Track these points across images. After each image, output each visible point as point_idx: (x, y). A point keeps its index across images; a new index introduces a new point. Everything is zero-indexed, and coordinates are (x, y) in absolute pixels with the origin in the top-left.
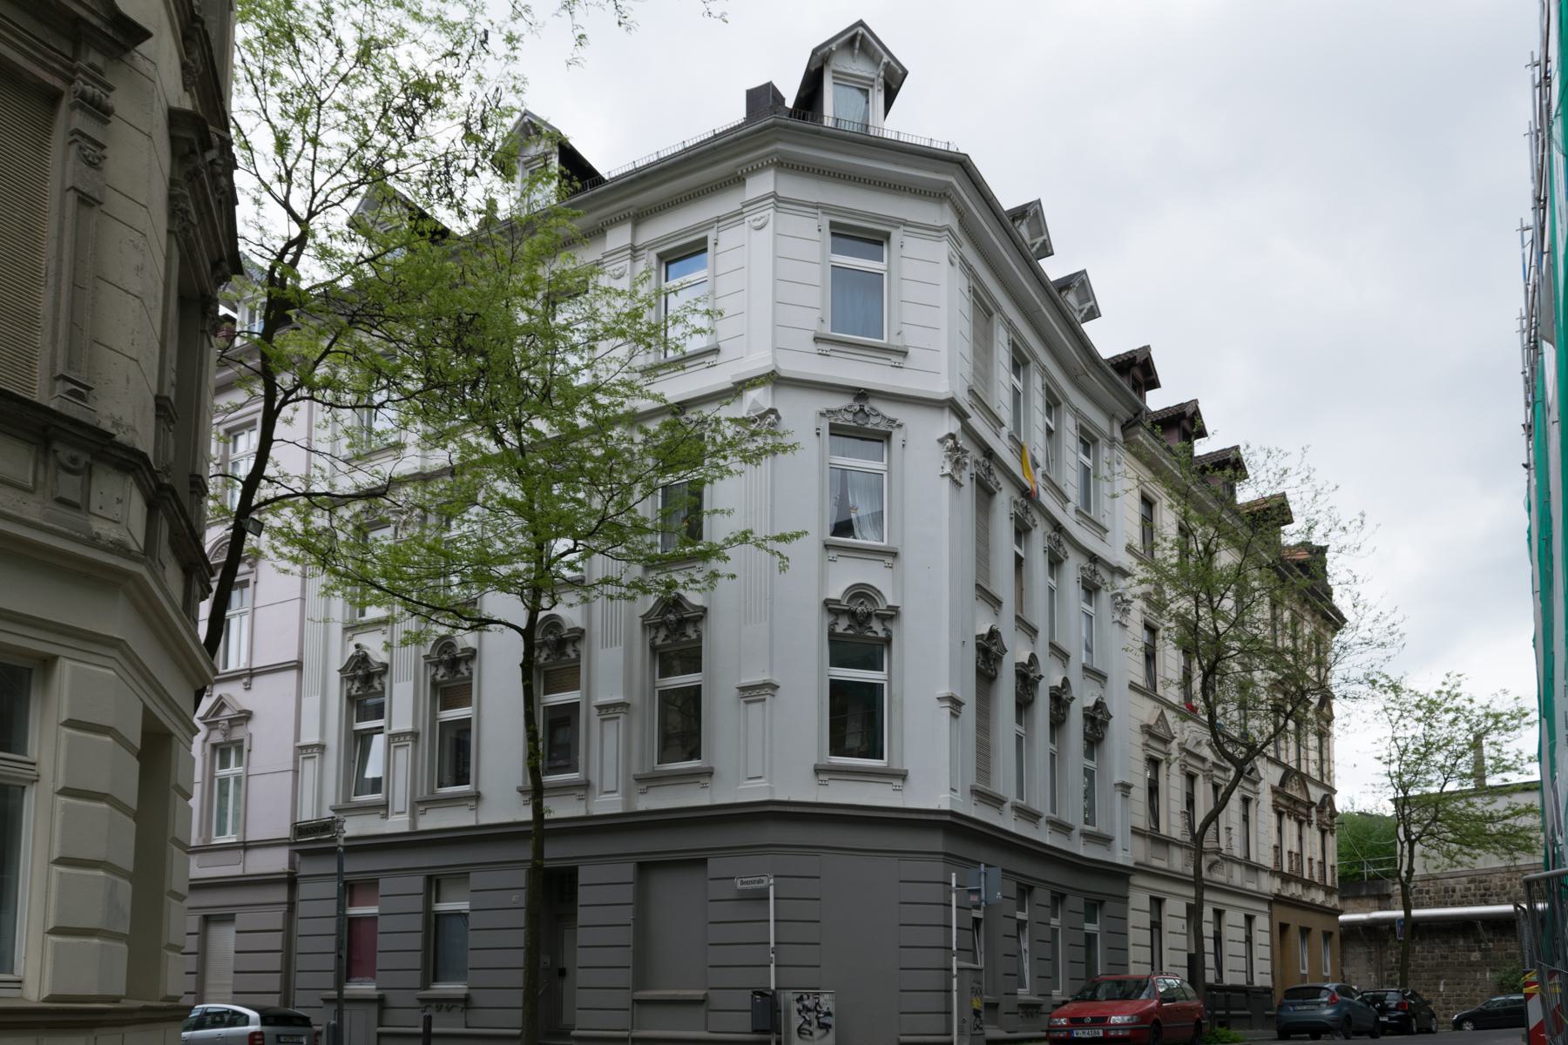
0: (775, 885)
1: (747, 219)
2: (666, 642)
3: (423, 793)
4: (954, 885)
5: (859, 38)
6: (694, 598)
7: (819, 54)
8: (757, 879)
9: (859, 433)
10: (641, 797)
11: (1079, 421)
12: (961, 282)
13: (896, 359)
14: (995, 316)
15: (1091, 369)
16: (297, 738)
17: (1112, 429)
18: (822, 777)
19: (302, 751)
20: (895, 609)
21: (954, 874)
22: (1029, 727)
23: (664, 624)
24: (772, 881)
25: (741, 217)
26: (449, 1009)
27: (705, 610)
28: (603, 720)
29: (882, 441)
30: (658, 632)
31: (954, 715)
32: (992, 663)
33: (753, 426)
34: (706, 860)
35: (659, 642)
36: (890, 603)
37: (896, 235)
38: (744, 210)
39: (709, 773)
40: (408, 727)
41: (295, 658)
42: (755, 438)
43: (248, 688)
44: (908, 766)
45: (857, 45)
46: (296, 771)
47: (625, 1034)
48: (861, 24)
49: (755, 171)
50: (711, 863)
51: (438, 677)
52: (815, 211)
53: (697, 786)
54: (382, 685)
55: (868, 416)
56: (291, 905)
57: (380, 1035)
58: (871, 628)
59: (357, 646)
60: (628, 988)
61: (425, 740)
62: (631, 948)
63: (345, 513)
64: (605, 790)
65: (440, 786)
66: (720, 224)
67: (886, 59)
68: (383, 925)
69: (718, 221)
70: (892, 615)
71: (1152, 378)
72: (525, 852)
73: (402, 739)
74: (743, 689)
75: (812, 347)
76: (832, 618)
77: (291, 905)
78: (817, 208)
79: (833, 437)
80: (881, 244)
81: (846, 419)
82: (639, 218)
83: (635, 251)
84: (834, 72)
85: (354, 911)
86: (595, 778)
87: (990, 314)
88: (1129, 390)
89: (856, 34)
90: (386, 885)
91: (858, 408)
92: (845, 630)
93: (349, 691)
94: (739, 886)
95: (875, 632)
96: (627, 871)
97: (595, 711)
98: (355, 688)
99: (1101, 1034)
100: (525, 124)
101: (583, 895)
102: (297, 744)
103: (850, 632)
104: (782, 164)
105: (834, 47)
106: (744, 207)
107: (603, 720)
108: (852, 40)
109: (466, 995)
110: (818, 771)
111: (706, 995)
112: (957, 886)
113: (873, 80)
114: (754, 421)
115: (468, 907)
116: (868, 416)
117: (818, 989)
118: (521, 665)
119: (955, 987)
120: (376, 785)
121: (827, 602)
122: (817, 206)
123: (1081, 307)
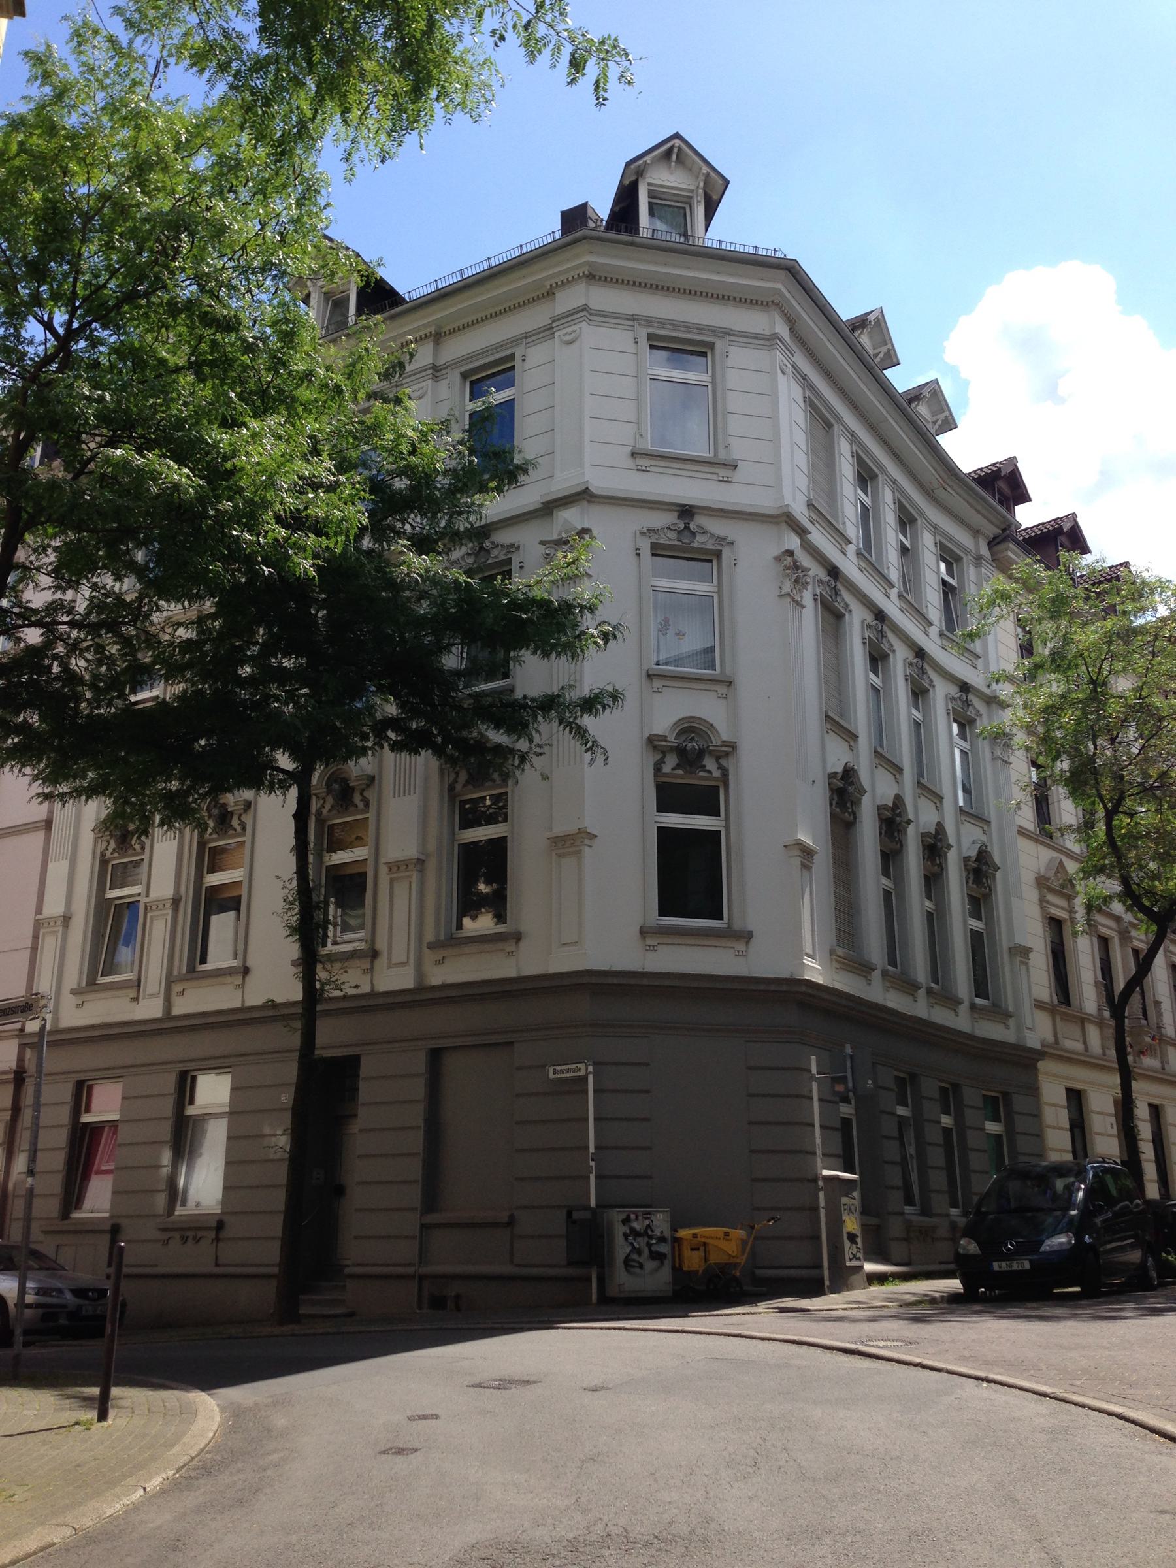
0: (595, 1074)
1: (556, 334)
5: (675, 150)
11: (938, 538)
12: (797, 392)
13: (724, 473)
18: (650, 941)
24: (591, 1069)
31: (806, 867)
37: (719, 344)
38: (554, 325)
45: (674, 157)
46: (34, 949)
48: (677, 136)
52: (631, 323)
64: (394, 961)
69: (526, 338)
75: (630, 463)
78: (633, 320)
80: (704, 355)
84: (649, 184)
86: (381, 944)
87: (829, 426)
89: (673, 147)
91: (682, 526)
94: (551, 1076)
95: (710, 772)
98: (328, 807)
103: (680, 772)
104: (594, 277)
118: (293, 816)
122: (633, 318)
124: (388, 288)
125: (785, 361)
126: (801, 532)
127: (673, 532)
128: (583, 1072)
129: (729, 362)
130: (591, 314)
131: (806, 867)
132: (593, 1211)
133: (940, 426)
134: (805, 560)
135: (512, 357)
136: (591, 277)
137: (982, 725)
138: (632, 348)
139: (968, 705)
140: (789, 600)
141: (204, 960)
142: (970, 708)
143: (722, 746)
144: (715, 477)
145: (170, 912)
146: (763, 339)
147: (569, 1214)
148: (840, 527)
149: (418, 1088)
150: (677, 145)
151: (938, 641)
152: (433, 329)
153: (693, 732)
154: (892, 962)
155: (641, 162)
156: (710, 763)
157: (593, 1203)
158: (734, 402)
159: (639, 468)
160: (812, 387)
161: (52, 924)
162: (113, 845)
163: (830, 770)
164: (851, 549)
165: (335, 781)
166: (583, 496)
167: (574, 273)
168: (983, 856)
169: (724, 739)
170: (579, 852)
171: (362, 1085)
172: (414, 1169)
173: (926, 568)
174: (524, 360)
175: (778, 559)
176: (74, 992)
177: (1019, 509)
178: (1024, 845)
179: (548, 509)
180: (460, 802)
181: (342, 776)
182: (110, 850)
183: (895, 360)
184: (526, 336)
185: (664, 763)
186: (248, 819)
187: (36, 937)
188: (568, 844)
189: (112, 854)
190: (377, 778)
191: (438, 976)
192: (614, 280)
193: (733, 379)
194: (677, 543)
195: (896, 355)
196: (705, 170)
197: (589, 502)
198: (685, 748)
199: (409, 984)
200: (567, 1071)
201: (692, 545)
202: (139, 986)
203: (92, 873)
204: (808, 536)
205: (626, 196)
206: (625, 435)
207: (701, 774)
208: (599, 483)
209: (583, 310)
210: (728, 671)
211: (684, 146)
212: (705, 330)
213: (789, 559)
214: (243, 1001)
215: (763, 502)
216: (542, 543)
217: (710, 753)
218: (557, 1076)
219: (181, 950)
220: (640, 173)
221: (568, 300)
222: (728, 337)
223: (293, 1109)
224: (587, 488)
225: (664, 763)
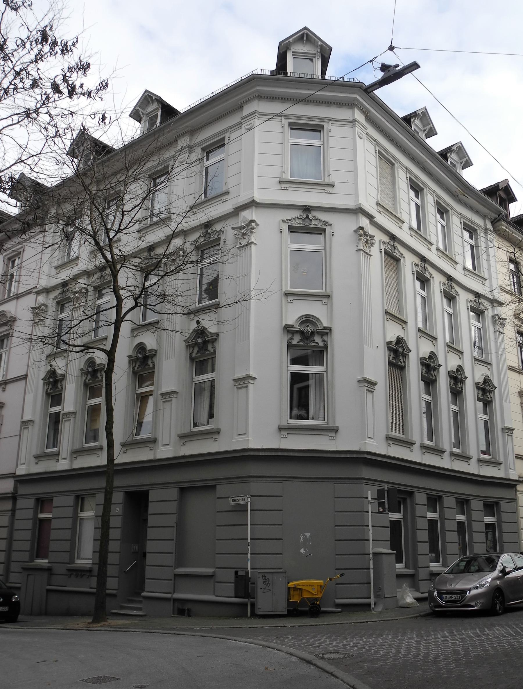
1: (243, 126)
3: (77, 447)
4: (370, 499)
5: (305, 35)
6: (212, 329)
8: (241, 498)
9: (307, 230)
10: (183, 447)
11: (462, 220)
12: (371, 147)
13: (327, 189)
14: (396, 165)
15: (465, 191)
16: (22, 418)
17: (485, 223)
18: (283, 433)
19: (25, 424)
20: (330, 329)
22: (435, 397)
23: (196, 344)
24: (249, 499)
25: (240, 125)
26: (82, 576)
27: (217, 335)
29: (321, 234)
30: (193, 350)
32: (401, 358)
33: (243, 231)
34: (215, 485)
35: (194, 355)
36: (325, 324)
37: (326, 125)
38: (242, 121)
39: (218, 432)
41: (25, 373)
42: (244, 237)
43: (4, 390)
44: (338, 423)
45: (305, 38)
47: (169, 596)
48: (306, 28)
49: (248, 101)
50: (55, 499)
52: (280, 118)
53: (212, 440)
55: (311, 220)
56: (13, 511)
57: (48, 591)
58: (314, 340)
60: (172, 566)
61: (79, 416)
62: (175, 541)
63: (52, 295)
64: (163, 444)
66: (231, 130)
67: (320, 43)
68: (54, 524)
69: (230, 129)
70: (327, 331)
71: (511, 196)
74: (236, 380)
75: (278, 186)
76: (290, 336)
77: (13, 511)
79: (291, 233)
80: (319, 131)
81: (299, 223)
82: (193, 132)
83: (191, 149)
84: (293, 52)
87: (393, 164)
88: (498, 206)
89: (304, 33)
90: (57, 501)
91: (305, 217)
93: (47, 391)
94: (232, 503)
95: (317, 343)
96: (173, 493)
97: (160, 396)
100: (146, 96)
101: (152, 508)
102: (22, 420)
103: (302, 343)
104: (261, 97)
105: (291, 40)
106: (242, 120)
108: (302, 36)
109: (90, 568)
111: (214, 572)
112: (371, 498)
113: (315, 54)
114: (244, 228)
115: (93, 514)
116: (311, 220)
119: (371, 566)
121: (286, 327)
123: (461, 161)
125: (361, 132)
126: (370, 217)
127: (300, 220)
129: (330, 134)
130: (260, 115)
133: (464, 165)
134: (371, 230)
135: (224, 139)
137: (489, 313)
138: (280, 130)
139: (480, 304)
140: (362, 252)
142: (481, 306)
143: (324, 329)
144: (323, 191)
146: (349, 122)
147: (236, 573)
148: (399, 215)
150: (305, 32)
151: (462, 272)
153: (308, 322)
154: (430, 439)
156: (318, 339)
158: (333, 153)
159: (283, 188)
160: (380, 145)
163: (388, 340)
164: (405, 226)
166: (252, 204)
168: (486, 381)
170: (247, 387)
173: (455, 235)
175: (356, 231)
177: (512, 206)
178: (512, 375)
183: (435, 132)
185: (293, 339)
188: (68, 416)
192: (266, 97)
193: (332, 142)
195: (435, 130)
197: (256, 207)
198: (304, 331)
200: (239, 500)
201: (310, 226)
204: (375, 219)
206: (275, 173)
207: (313, 344)
208: (259, 197)
209: (255, 113)
210: (328, 291)
211: (308, 32)
213: (361, 231)
215: (348, 203)
216: (233, 228)
218: (234, 503)
221: (248, 110)
222: (330, 122)
224: (254, 200)
225: (293, 339)
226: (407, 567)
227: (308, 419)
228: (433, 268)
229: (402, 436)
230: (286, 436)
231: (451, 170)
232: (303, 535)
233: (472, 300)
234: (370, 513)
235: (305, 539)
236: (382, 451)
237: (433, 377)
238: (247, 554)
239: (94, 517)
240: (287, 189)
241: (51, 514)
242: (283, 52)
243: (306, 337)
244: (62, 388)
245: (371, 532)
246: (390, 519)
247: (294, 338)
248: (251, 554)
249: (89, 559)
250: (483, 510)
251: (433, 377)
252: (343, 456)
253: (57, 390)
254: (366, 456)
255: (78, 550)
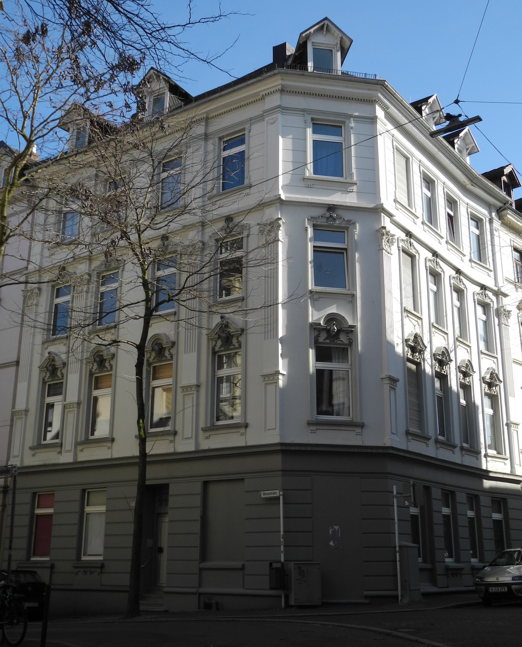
0: (284, 496)
1: (266, 119)
2: (221, 349)
4: (395, 493)
5: (325, 26)
7: (304, 35)
21: (394, 486)
24: (281, 493)
25: (262, 118)
28: (266, 384)
31: (393, 388)
38: (264, 114)
40: (194, 382)
45: (325, 29)
46: (12, 426)
51: (151, 360)
54: (62, 375)
59: (49, 353)
64: (185, 437)
65: (218, 420)
68: (55, 520)
72: (134, 473)
73: (189, 389)
74: (264, 376)
76: (317, 333)
78: (304, 111)
81: (322, 222)
83: (206, 137)
84: (313, 43)
85: (38, 511)
86: (178, 428)
92: (324, 340)
94: (263, 496)
98: (152, 357)
99: (506, 590)
103: (328, 341)
105: (312, 30)
107: (266, 384)
110: (309, 424)
112: (397, 493)
117: (312, 561)
118: (135, 366)
119: (398, 559)
120: (163, 422)
122: (304, 110)
124: (184, 92)
128: (277, 495)
130: (283, 109)
131: (393, 388)
132: (283, 564)
136: (282, 91)
141: (92, 434)
145: (76, 409)
147: (271, 565)
149: (197, 501)
150: (326, 23)
152: (205, 116)
154: (442, 434)
155: (308, 32)
156: (343, 338)
157: (282, 560)
159: (307, 186)
161: (20, 414)
162: (48, 374)
165: (156, 344)
167: (274, 89)
168: (493, 375)
169: (350, 324)
171: (171, 499)
172: (196, 541)
174: (249, 132)
176: (31, 448)
179: (262, 206)
180: (218, 355)
181: (159, 342)
182: (47, 377)
184: (251, 119)
185: (320, 337)
186: (113, 363)
187: (12, 420)
189: (48, 379)
190: (176, 343)
191: (206, 444)
194: (326, 224)
196: (340, 35)
199: (192, 448)
200: (270, 494)
202: (62, 446)
203: (38, 390)
204: (394, 218)
205: (302, 47)
207: (338, 342)
212: (341, 115)
214: (112, 455)
217: (343, 331)
218: (265, 496)
219: (82, 422)
220: (308, 37)
223: (135, 510)
225: (320, 337)
226: (424, 561)
227: (332, 414)
228: (443, 262)
229: (419, 431)
230: (315, 431)
231: (462, 161)
232: (332, 528)
233: (479, 292)
234: (395, 508)
235: (334, 531)
236: (402, 446)
237: (495, 393)
238: (280, 546)
239: (105, 511)
240: (311, 186)
241: (53, 509)
242: (303, 42)
243: (334, 336)
244: (63, 376)
245: (396, 526)
246: (411, 513)
247: (320, 335)
248: (284, 546)
249: (100, 555)
250: (491, 505)
251: (495, 393)
252: (369, 451)
253: (57, 378)
254: (391, 451)
255: (84, 547)
